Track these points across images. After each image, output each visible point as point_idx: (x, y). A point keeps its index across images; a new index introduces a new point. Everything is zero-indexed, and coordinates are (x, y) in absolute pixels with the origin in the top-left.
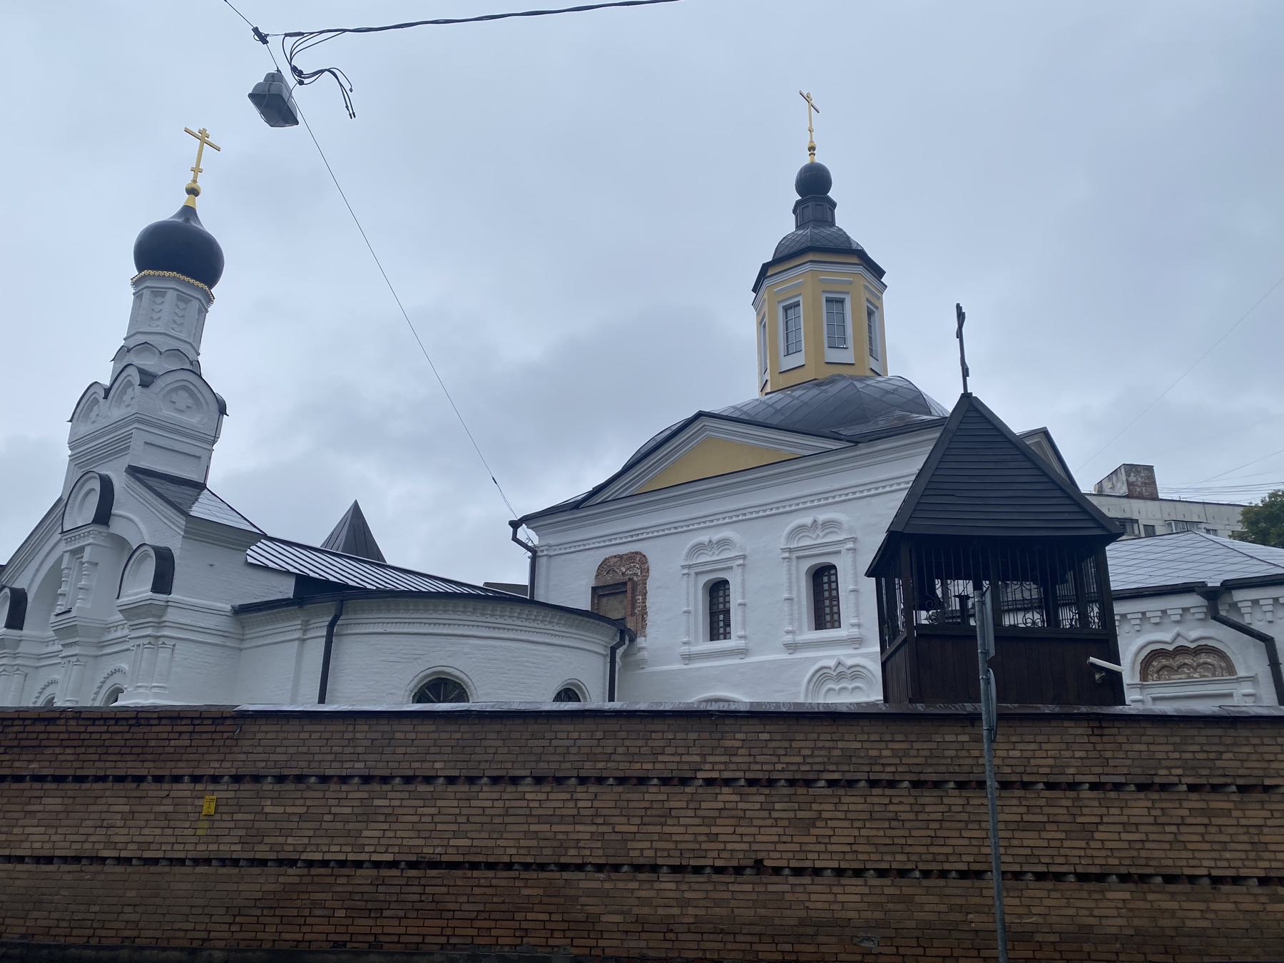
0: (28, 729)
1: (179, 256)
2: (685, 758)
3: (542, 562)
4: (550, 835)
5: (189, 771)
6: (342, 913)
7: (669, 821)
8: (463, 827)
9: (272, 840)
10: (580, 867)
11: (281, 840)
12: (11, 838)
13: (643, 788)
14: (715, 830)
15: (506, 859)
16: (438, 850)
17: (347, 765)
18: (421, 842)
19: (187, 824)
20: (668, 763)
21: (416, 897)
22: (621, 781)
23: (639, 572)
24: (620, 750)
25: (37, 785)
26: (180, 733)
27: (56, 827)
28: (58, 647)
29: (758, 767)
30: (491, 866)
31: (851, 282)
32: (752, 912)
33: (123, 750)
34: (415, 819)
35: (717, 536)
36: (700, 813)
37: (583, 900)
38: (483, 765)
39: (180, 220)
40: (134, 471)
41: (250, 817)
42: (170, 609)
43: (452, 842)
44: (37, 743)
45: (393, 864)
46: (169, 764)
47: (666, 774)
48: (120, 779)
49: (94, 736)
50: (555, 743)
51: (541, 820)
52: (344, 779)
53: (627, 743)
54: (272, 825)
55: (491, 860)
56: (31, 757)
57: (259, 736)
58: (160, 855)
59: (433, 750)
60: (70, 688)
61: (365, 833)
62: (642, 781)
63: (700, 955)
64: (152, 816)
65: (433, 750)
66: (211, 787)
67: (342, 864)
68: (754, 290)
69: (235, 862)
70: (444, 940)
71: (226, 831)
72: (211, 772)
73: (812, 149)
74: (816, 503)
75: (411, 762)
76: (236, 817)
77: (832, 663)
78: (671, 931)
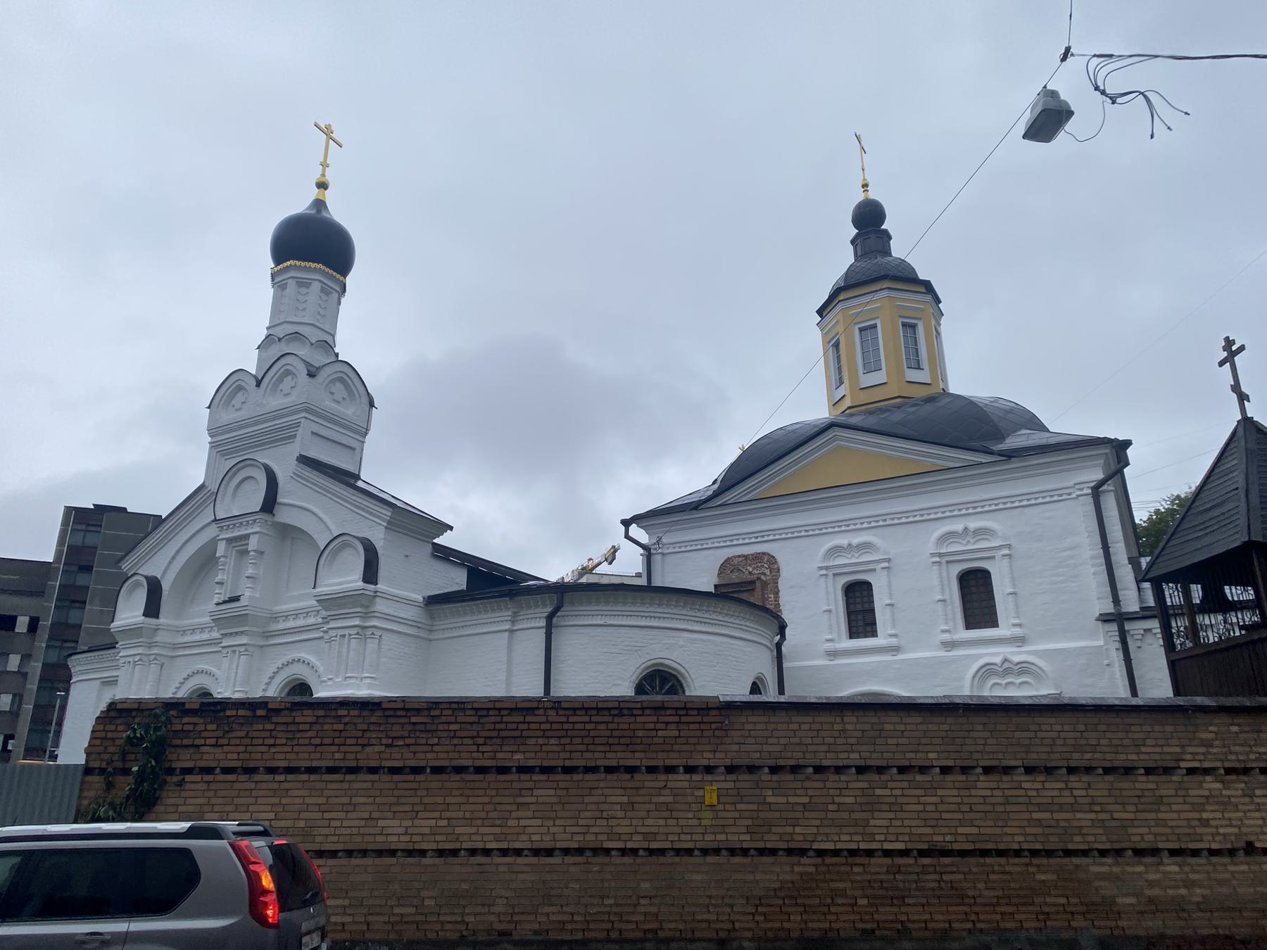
0: (505, 719)
1: (313, 248)
2: (1166, 749)
3: (657, 559)
4: (1053, 823)
5: (683, 762)
6: (864, 902)
7: (1162, 808)
8: (967, 816)
9: (779, 830)
10: (1084, 853)
11: (789, 829)
12: (504, 830)
13: (1131, 777)
14: (1205, 815)
15: (1016, 847)
16: (948, 838)
17: (842, 756)
18: (929, 830)
19: (690, 815)
20: (1150, 753)
21: (935, 885)
22: (1107, 771)
23: (768, 572)
24: (1104, 742)
25: (524, 777)
26: (667, 723)
27: (554, 819)
28: (215, 634)
29: (1233, 757)
30: (1001, 853)
31: (922, 310)
32: (1252, 890)
33: (611, 741)
34: (920, 808)
35: (857, 539)
36: (1189, 800)
37: (1096, 884)
38: (976, 756)
39: (313, 212)
40: (304, 460)
41: (754, 807)
42: (378, 600)
43: (960, 830)
44: (517, 733)
45: (905, 853)
46: (660, 755)
47: (1151, 765)
48: (610, 770)
49: (577, 726)
50: (1040, 735)
51: (1041, 807)
52: (839, 770)
53: (1109, 735)
54: (777, 815)
55: (1001, 847)
56: (515, 748)
57: (748, 727)
58: (668, 845)
59: (924, 741)
60: (232, 679)
61: (872, 822)
62: (1128, 771)
63: (1213, 931)
64: (652, 807)
65: (924, 741)
66: (709, 777)
67: (853, 853)
68: (821, 312)
69: (745, 852)
70: (970, 925)
71: (731, 822)
72: (706, 763)
73: (865, 186)
74: (964, 512)
75: (904, 752)
76: (739, 807)
77: (998, 660)
78: (1183, 910)
